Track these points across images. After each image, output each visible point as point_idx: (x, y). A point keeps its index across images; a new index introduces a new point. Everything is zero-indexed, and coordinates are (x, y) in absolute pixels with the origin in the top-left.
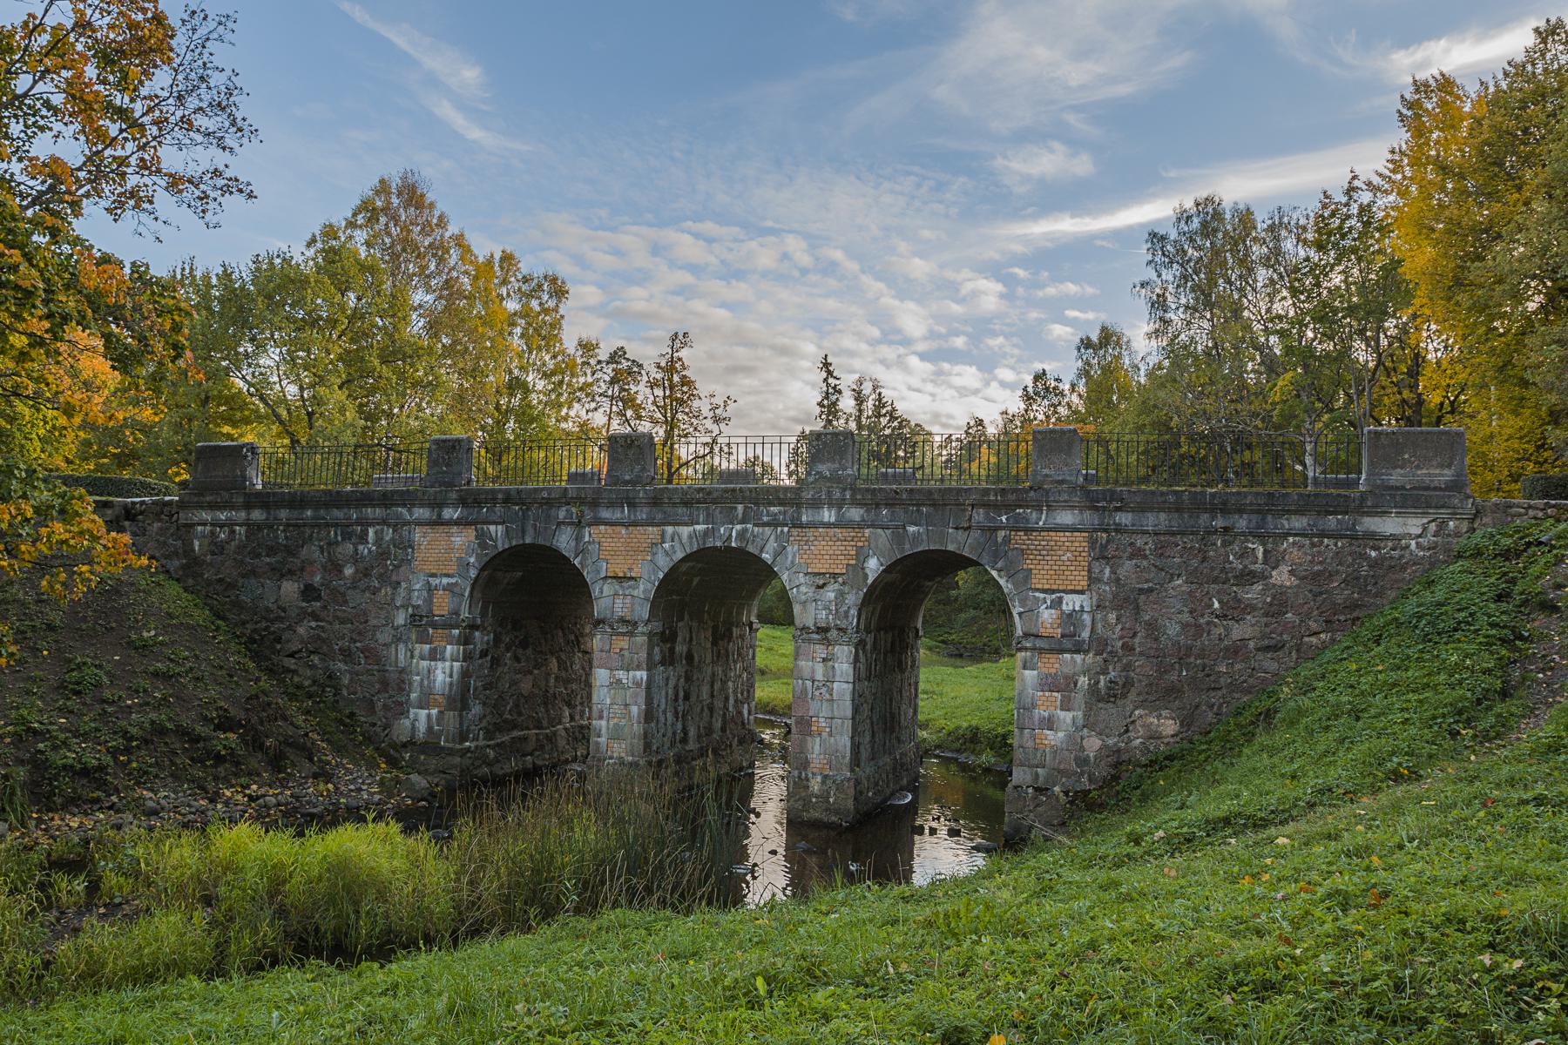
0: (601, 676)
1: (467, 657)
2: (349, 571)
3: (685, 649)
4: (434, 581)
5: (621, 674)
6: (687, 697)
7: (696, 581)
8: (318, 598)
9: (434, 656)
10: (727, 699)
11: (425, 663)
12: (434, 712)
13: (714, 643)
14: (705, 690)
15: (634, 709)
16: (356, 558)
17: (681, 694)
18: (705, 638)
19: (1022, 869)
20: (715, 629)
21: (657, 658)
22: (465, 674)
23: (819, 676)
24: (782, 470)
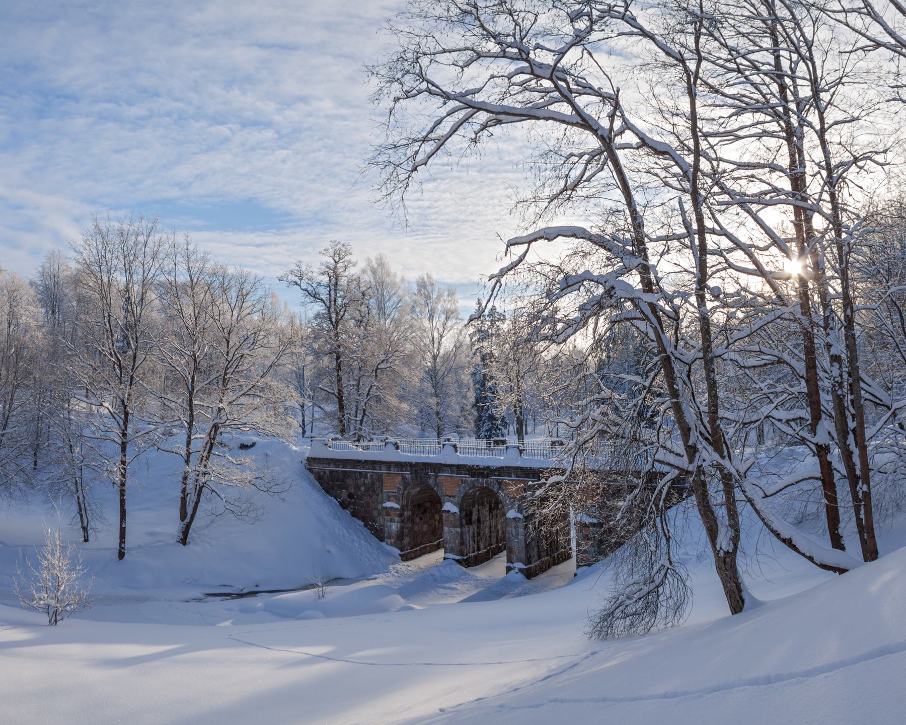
0: (446, 529)
1: (402, 521)
2: (362, 488)
3: (476, 518)
4: (390, 494)
5: (452, 529)
6: (479, 534)
7: (478, 493)
8: (354, 498)
9: (392, 521)
10: (498, 531)
11: (389, 523)
12: (393, 541)
13: (490, 512)
14: (487, 530)
15: (457, 541)
16: (364, 484)
17: (476, 534)
18: (485, 512)
19: (803, 122)
20: (490, 507)
21: (464, 523)
22: (402, 528)
23: (514, 533)
24: (809, 261)
